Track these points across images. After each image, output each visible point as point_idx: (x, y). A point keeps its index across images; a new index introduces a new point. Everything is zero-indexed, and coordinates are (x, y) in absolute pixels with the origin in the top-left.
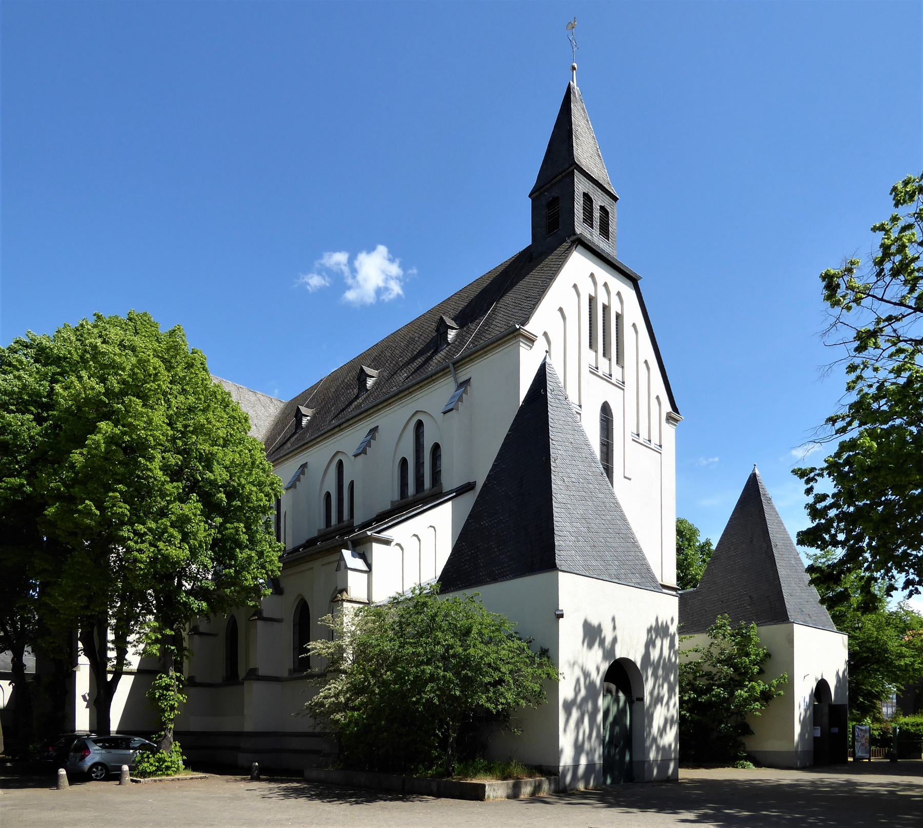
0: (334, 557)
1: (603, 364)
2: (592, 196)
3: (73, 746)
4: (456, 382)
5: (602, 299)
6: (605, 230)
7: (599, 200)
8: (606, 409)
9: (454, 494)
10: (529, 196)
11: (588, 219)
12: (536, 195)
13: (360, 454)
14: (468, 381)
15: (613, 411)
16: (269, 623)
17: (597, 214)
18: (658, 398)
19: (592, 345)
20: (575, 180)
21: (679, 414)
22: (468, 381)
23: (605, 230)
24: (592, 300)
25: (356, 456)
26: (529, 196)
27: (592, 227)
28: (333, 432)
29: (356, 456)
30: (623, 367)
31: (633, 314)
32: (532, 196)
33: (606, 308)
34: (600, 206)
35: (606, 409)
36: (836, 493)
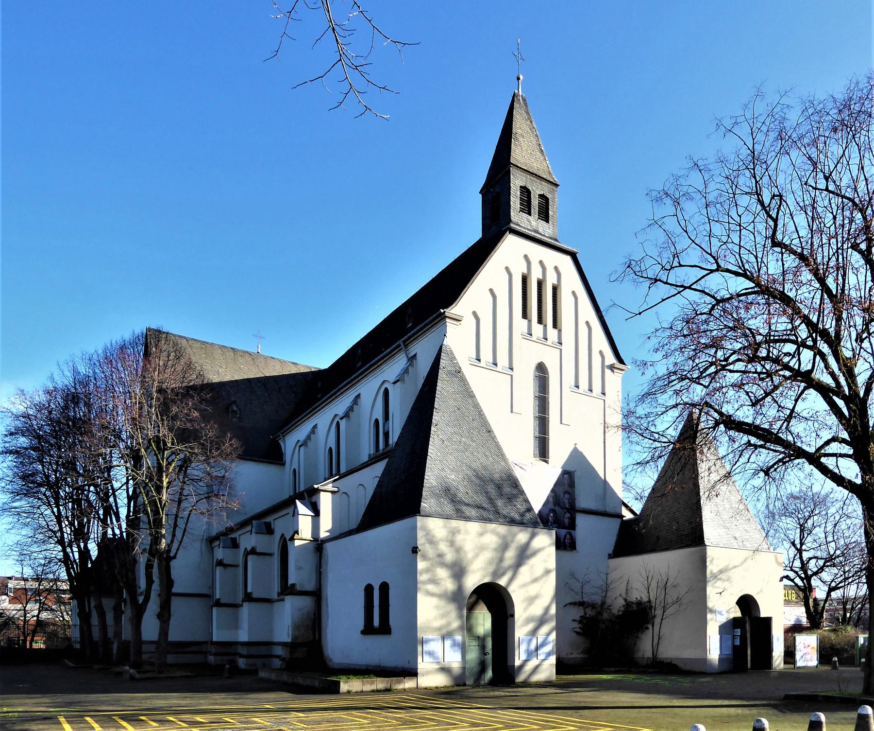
0: (290, 510)
1: (537, 329)
2: (530, 188)
3: (114, 657)
4: (407, 357)
5: (536, 274)
6: (544, 215)
7: (537, 189)
8: (541, 368)
9: (337, 477)
10: (480, 193)
11: (526, 207)
12: (484, 192)
13: (398, 381)
14: (415, 355)
15: (549, 370)
16: (262, 557)
17: (535, 202)
18: (601, 352)
19: (525, 315)
20: (512, 177)
21: (624, 364)
22: (415, 355)
23: (544, 215)
24: (525, 280)
25: (395, 383)
26: (480, 193)
27: (529, 214)
28: (392, 354)
29: (395, 383)
30: (560, 331)
31: (571, 282)
32: (483, 192)
33: (540, 284)
34: (539, 195)
35: (541, 368)
36: (159, 613)
